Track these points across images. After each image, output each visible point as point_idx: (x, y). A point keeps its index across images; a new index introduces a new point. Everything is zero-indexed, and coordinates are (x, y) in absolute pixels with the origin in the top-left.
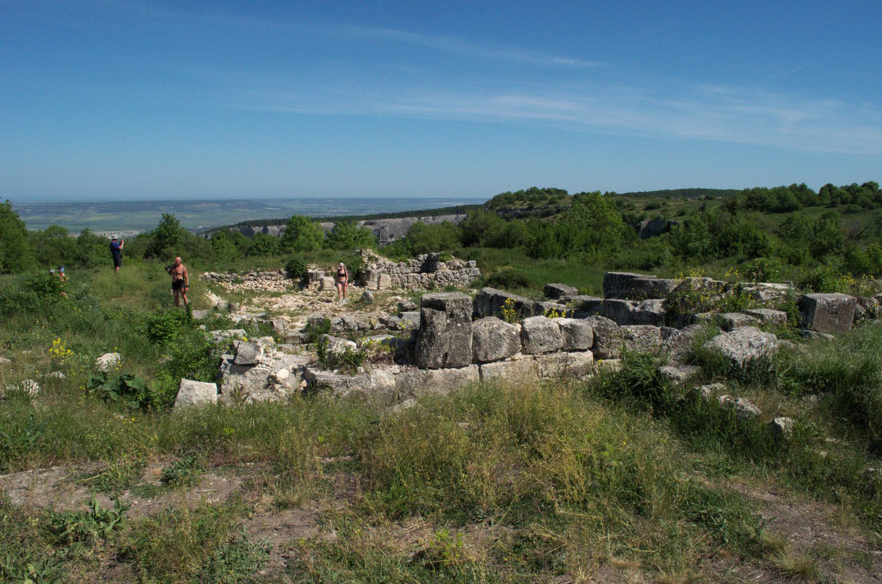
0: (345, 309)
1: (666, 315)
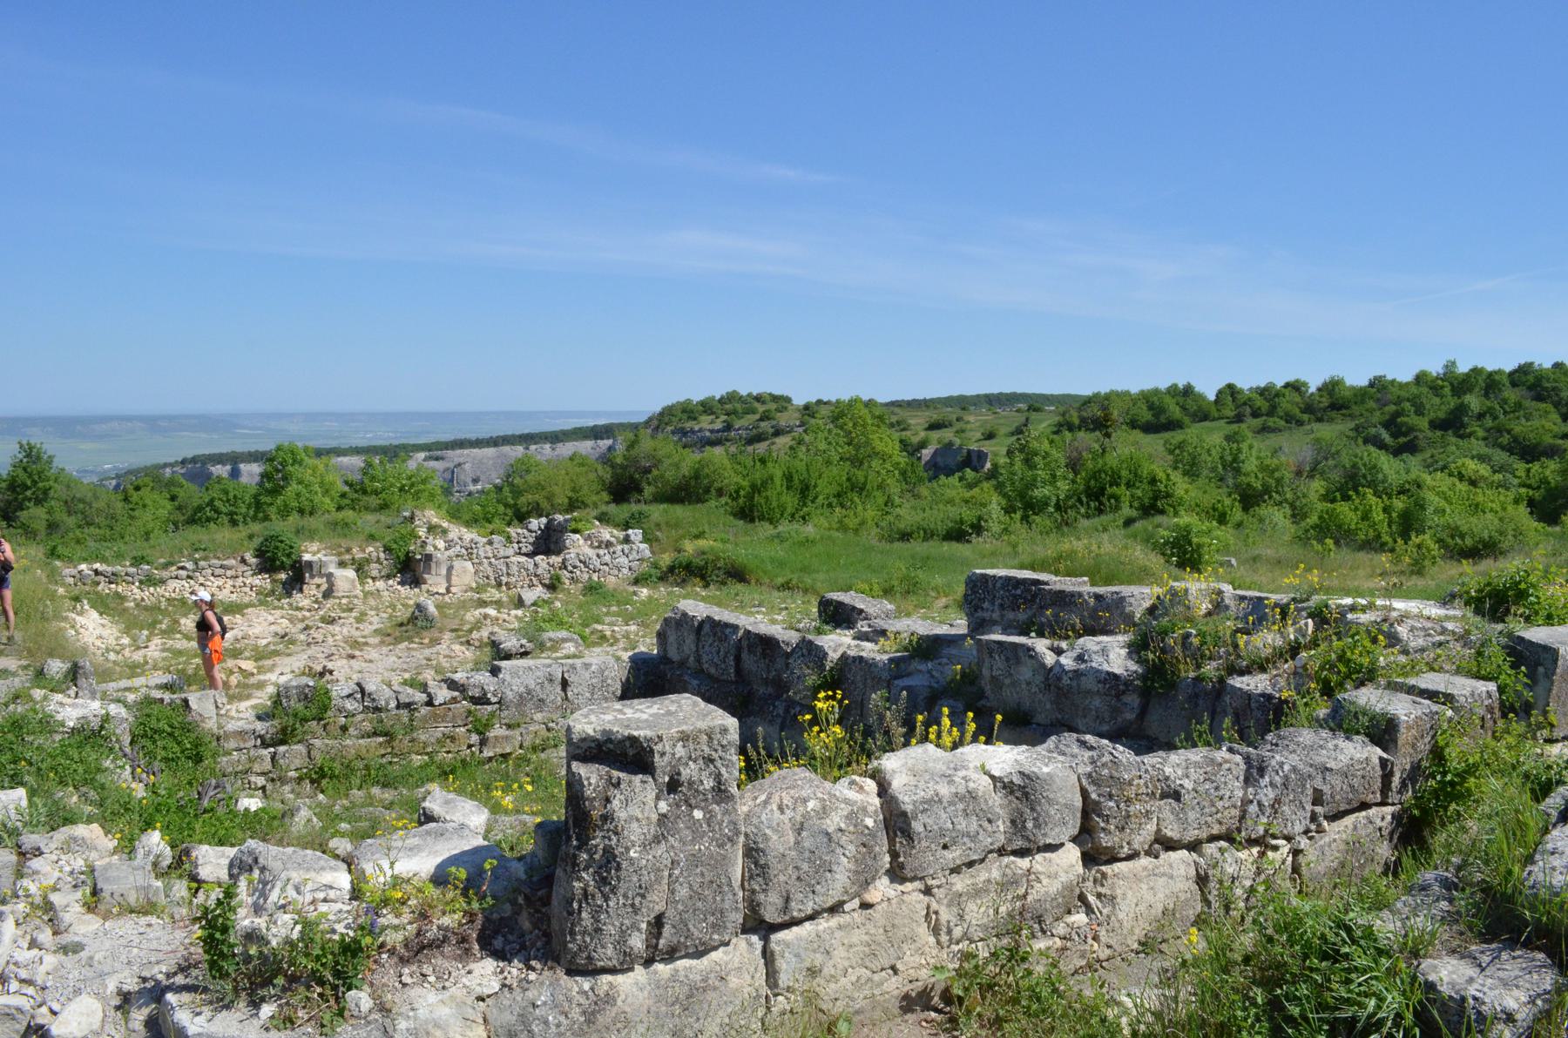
0: (374, 640)
1: (1144, 678)
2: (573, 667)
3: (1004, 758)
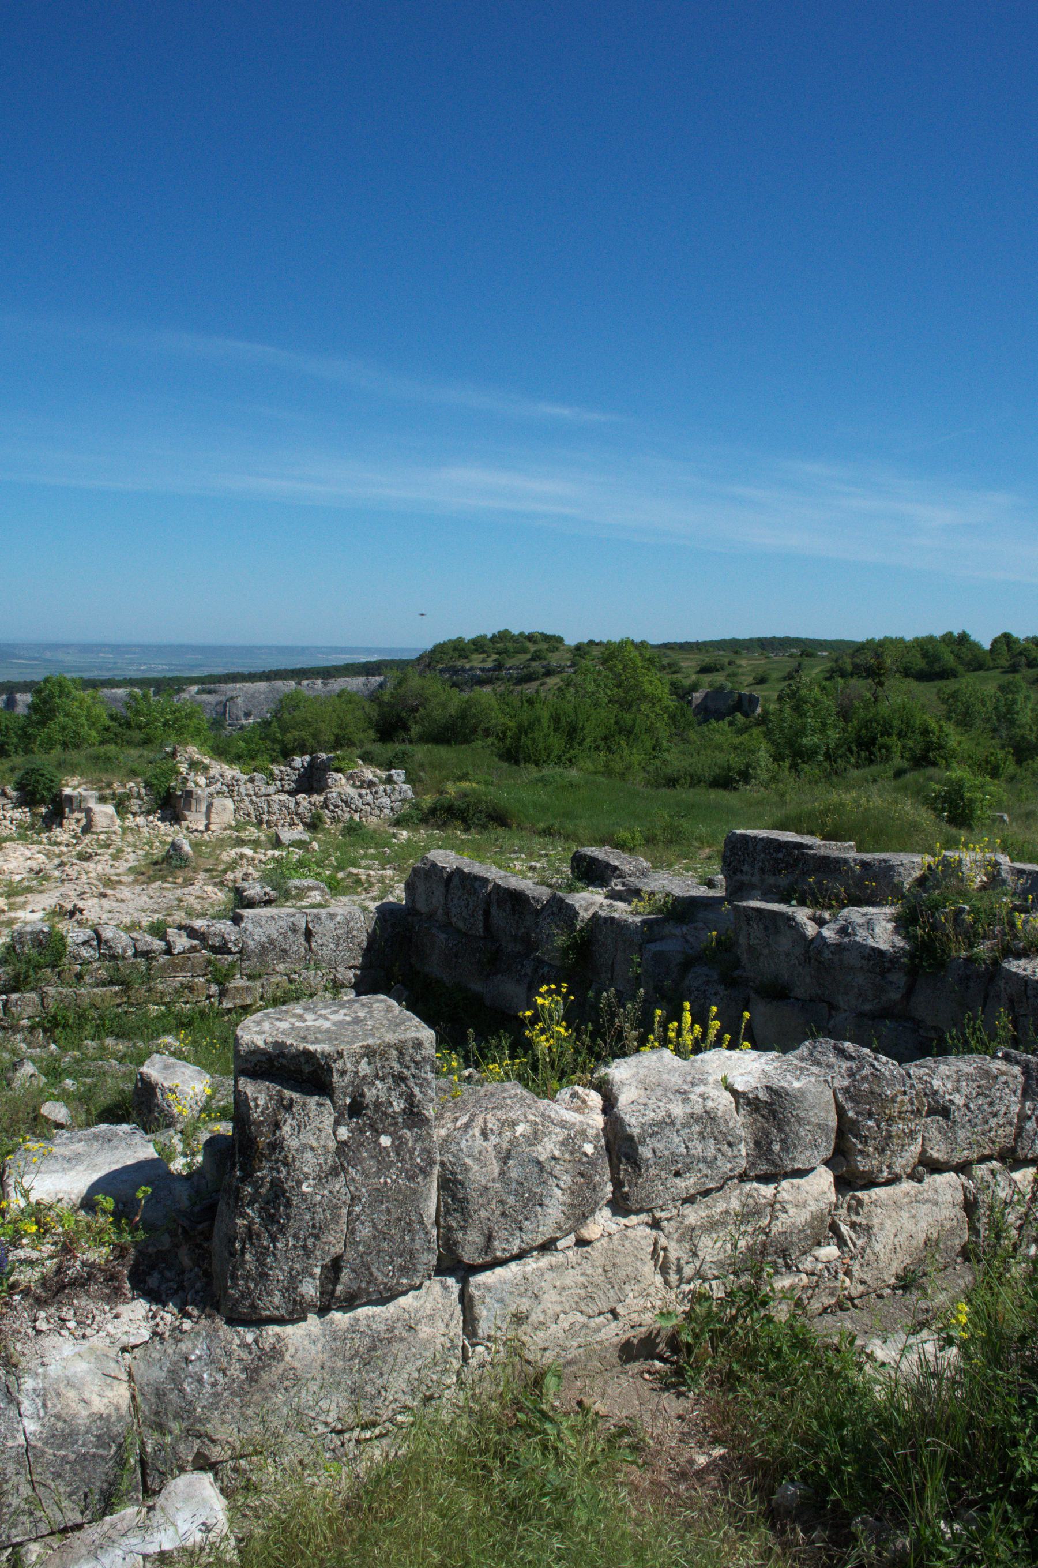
1: (911, 955)
2: (318, 917)
3: (748, 1067)
